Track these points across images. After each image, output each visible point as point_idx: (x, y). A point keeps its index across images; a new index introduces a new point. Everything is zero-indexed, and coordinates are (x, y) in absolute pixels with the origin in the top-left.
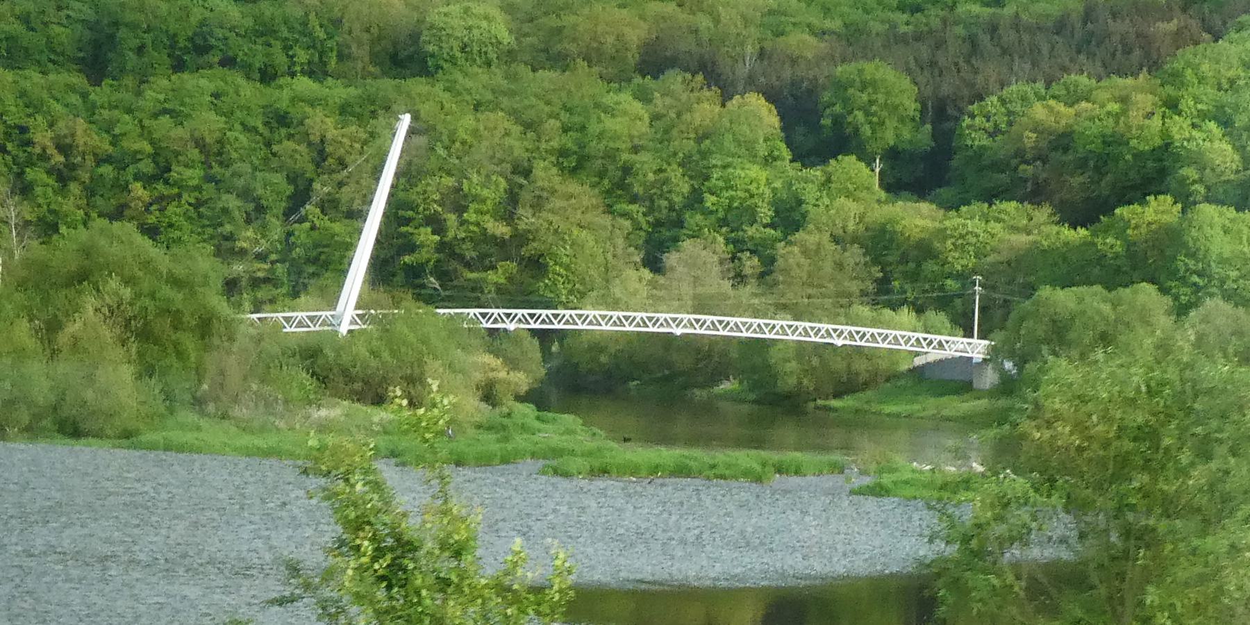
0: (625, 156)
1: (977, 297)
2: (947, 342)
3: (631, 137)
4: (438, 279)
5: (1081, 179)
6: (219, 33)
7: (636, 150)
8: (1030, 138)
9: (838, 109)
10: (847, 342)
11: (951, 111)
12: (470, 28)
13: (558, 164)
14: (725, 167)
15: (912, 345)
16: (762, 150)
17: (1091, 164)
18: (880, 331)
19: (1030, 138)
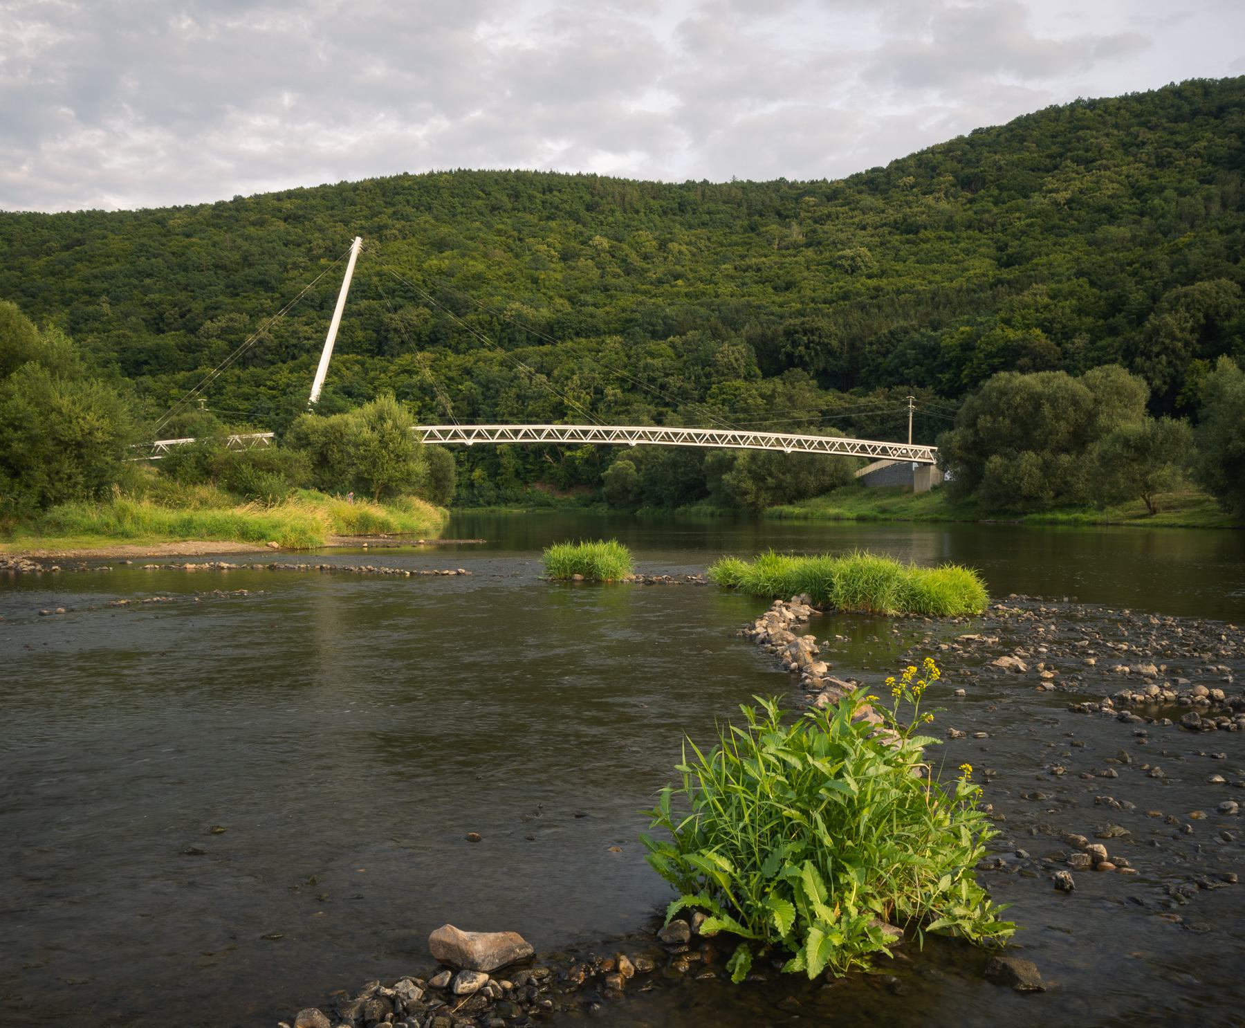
0: (660, 380)
1: (911, 414)
2: (891, 448)
3: (665, 368)
4: (551, 456)
5: (947, 376)
6: (443, 331)
7: (667, 375)
8: (911, 353)
9: (789, 348)
10: (797, 450)
11: (858, 344)
12: (580, 322)
13: (621, 387)
14: (719, 382)
15: (857, 452)
16: (742, 371)
17: (954, 364)
18: (828, 439)
19: (911, 353)
